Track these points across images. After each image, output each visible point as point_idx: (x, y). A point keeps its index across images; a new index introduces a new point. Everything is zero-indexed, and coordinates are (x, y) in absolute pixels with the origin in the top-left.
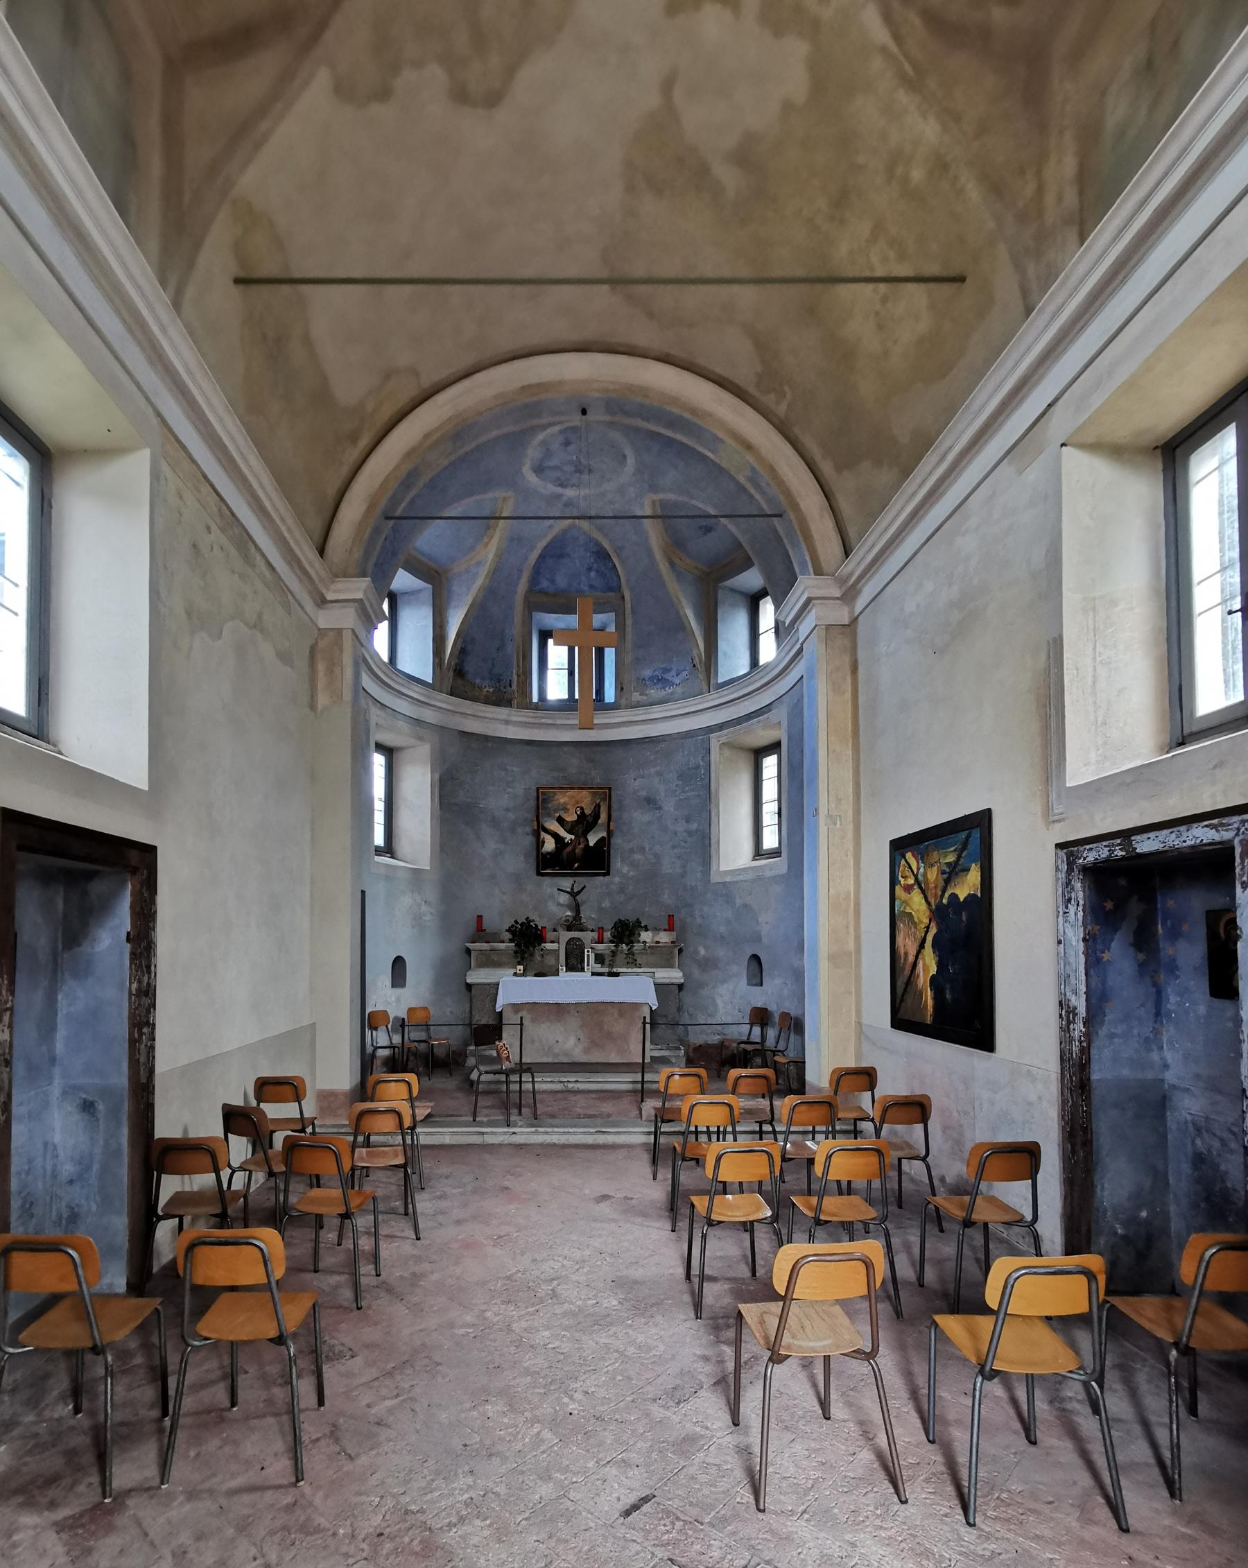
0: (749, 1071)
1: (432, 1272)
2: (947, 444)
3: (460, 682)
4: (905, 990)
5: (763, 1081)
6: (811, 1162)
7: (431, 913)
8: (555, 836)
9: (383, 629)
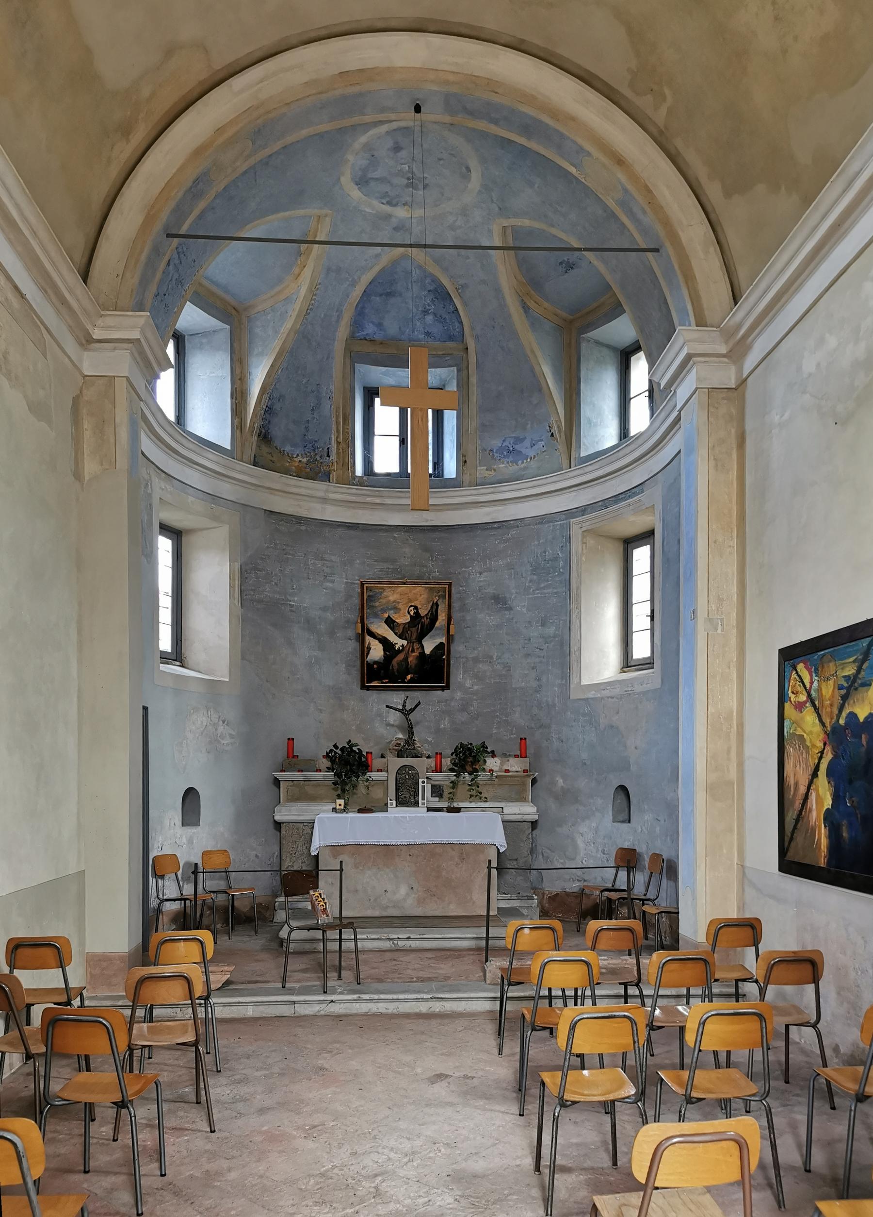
0: (613, 923)
1: (230, 1170)
2: (855, 167)
3: (265, 449)
4: (795, 828)
5: (628, 934)
6: (682, 1029)
7: (230, 735)
8: (384, 641)
9: (166, 382)
